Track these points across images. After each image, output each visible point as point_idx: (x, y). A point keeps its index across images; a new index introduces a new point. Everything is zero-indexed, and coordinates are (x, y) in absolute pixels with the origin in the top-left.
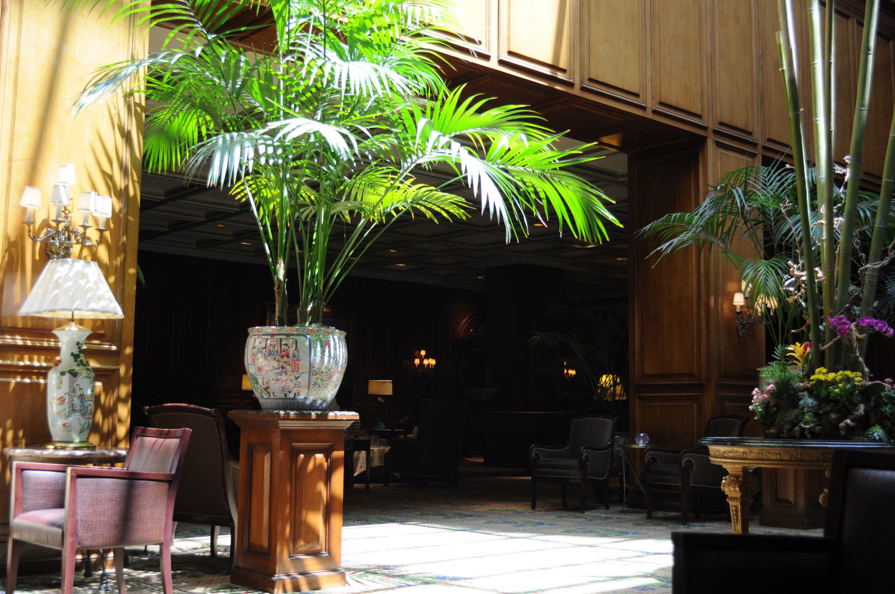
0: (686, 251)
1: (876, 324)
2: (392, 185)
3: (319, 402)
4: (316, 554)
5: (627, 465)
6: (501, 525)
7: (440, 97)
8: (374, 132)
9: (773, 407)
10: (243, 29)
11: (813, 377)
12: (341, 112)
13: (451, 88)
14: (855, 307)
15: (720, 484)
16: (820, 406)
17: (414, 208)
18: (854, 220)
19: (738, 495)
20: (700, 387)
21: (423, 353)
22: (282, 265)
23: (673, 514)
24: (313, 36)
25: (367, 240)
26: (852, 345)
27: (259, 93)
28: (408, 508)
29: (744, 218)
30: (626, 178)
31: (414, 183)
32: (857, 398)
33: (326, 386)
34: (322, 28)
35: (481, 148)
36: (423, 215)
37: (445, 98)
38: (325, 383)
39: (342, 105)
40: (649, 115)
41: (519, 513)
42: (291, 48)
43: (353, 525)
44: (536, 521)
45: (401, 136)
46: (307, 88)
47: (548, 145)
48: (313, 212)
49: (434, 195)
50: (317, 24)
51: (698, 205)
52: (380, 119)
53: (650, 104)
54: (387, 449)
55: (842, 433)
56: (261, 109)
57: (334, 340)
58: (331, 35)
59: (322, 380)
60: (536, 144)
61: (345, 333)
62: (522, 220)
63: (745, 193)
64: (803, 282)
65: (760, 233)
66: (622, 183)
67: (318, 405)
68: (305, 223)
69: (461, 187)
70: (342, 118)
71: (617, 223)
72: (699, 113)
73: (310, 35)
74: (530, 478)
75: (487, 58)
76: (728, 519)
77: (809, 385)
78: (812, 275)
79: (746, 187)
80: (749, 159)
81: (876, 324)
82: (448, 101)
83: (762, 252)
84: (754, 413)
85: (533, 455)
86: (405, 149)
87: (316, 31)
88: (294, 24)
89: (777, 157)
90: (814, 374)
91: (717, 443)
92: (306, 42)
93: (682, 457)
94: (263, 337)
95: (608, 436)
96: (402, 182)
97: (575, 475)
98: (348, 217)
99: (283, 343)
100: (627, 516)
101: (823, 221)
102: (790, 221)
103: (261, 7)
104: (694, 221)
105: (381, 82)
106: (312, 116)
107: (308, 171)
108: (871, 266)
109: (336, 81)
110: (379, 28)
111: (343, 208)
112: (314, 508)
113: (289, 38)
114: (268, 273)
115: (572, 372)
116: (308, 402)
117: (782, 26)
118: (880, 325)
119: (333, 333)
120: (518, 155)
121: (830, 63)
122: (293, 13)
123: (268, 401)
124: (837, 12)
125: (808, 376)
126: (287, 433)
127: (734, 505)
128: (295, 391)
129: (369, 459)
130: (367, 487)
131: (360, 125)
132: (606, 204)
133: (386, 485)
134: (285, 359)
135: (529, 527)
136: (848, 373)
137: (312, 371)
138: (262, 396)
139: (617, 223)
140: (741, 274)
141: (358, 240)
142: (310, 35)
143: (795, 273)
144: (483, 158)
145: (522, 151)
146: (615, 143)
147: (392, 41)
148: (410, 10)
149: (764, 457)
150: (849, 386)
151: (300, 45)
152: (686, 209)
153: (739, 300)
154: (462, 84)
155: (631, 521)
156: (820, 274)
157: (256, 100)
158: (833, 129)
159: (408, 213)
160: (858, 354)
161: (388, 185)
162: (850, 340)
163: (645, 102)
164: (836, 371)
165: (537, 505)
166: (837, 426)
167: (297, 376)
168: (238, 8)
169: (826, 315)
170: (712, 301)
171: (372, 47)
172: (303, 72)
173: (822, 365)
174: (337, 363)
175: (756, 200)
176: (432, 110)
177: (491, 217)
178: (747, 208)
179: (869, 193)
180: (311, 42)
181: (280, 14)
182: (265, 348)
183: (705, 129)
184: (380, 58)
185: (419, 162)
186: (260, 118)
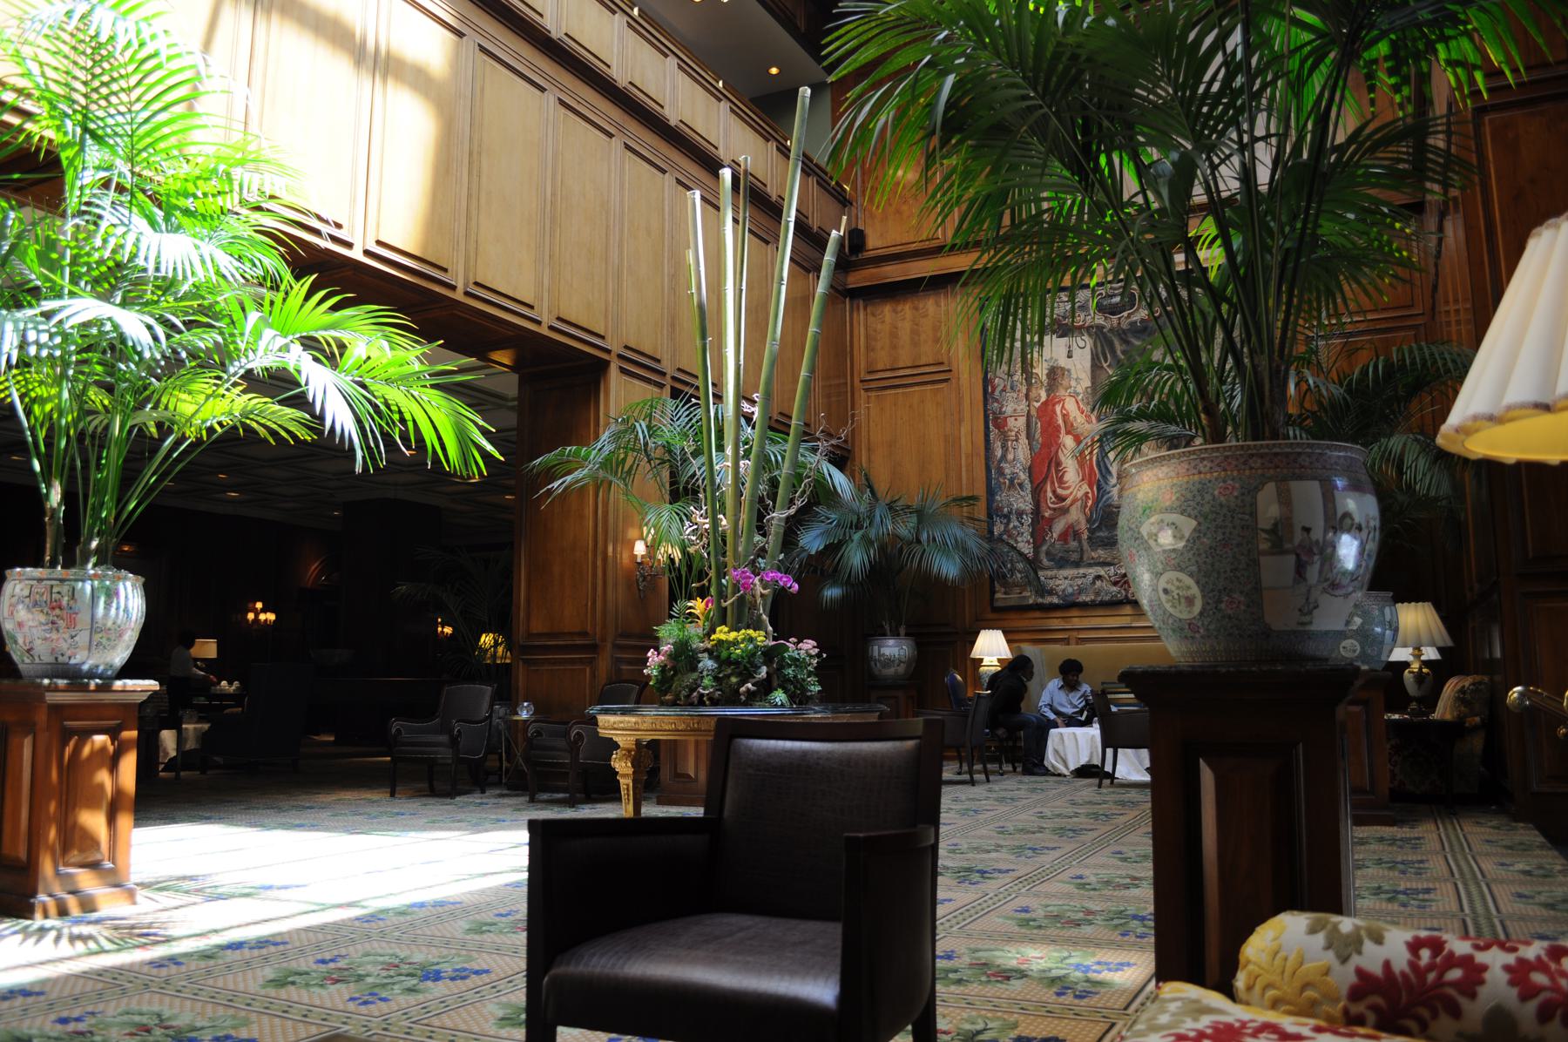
0: (582, 491)
1: (781, 578)
2: (214, 391)
3: (101, 668)
4: (94, 866)
5: (507, 740)
6: (350, 818)
7: (282, 288)
8: (189, 325)
9: (670, 670)
10: (16, 176)
11: (713, 637)
12: (149, 296)
13: (298, 278)
14: (760, 560)
15: (610, 760)
16: (720, 669)
17: (243, 424)
18: (764, 463)
19: (630, 771)
20: (594, 648)
21: (259, 605)
22: (59, 489)
23: (561, 796)
24: (116, 195)
25: (178, 460)
26: (756, 601)
27: (36, 260)
28: (231, 801)
29: (648, 456)
30: (516, 403)
31: (244, 392)
32: (759, 659)
33: (114, 647)
34: (129, 186)
35: (333, 354)
36: (255, 432)
37: (947, 248)
38: (112, 643)
39: (150, 287)
40: (544, 331)
41: (373, 802)
42: (84, 208)
43: (155, 825)
44: (492, 817)
45: (227, 331)
46: (101, 262)
47: (417, 357)
48: (106, 421)
49: (269, 408)
50: (121, 180)
51: (597, 437)
52: (202, 310)
53: (547, 319)
54: (206, 726)
55: (743, 698)
56: (39, 283)
57: (126, 589)
58: (140, 196)
59: (108, 639)
60: (400, 353)
61: (143, 579)
62: (378, 446)
63: (649, 428)
64: (706, 530)
65: (666, 474)
66: (512, 408)
67: (100, 671)
68: (93, 436)
69: (300, 401)
70: (147, 304)
71: (497, 455)
72: (602, 334)
73: (112, 194)
74: (389, 759)
75: (349, 245)
76: (619, 799)
77: (709, 646)
78: (715, 523)
79: (650, 421)
80: (656, 390)
81: (781, 578)
82: (292, 294)
83: (667, 497)
84: (649, 677)
85: (394, 731)
86: (232, 347)
87: (121, 189)
88: (89, 177)
89: (686, 389)
90: (715, 633)
91: (606, 712)
92: (106, 202)
93: (571, 728)
94: (27, 582)
95: (485, 705)
96: (228, 390)
97: (444, 754)
98: (153, 430)
99: (55, 590)
100: (506, 801)
101: (729, 464)
102: (696, 463)
103: (47, 151)
104: (592, 457)
105: (203, 262)
106: (106, 297)
107: (99, 368)
108: (778, 516)
109: (142, 255)
110: (205, 195)
111: (149, 419)
112: (93, 804)
113: (80, 196)
114: (40, 500)
115: (448, 630)
116: (85, 667)
117: (692, 245)
118: (785, 579)
119: (126, 578)
120: (380, 366)
121: (741, 290)
122: (89, 164)
123: (31, 667)
124: (750, 231)
125: (708, 635)
126: (57, 709)
127: (625, 783)
128: (69, 653)
129: (180, 741)
130: (178, 775)
131: (174, 315)
132: (485, 432)
133: (203, 772)
134: (57, 611)
135: (385, 818)
136: (751, 632)
137: (94, 628)
138: (23, 661)
139: (497, 455)
140: (643, 519)
141: (162, 463)
142: (112, 194)
143: (698, 519)
144: (335, 366)
145: (385, 361)
146: (506, 361)
147: (222, 213)
148: (247, 177)
149: (658, 727)
150: (751, 647)
151: (98, 206)
152: (583, 441)
153: (640, 549)
154: (312, 274)
155: (510, 806)
156: (724, 522)
157: (34, 273)
158: (742, 362)
159: (235, 428)
160: (761, 611)
161: (209, 392)
162: (754, 596)
163: (541, 316)
164: (738, 630)
165: (397, 792)
166: (737, 691)
167: (74, 634)
168: (10, 148)
169: (730, 568)
170: (610, 549)
171: (195, 217)
172: (98, 242)
173: (724, 623)
174: (128, 617)
175: (662, 436)
176: (272, 303)
177: (337, 440)
178: (651, 445)
179: (782, 435)
180: (113, 203)
181: (71, 162)
182: (29, 596)
183: (608, 351)
184: (205, 232)
185: (249, 366)
186: (35, 292)
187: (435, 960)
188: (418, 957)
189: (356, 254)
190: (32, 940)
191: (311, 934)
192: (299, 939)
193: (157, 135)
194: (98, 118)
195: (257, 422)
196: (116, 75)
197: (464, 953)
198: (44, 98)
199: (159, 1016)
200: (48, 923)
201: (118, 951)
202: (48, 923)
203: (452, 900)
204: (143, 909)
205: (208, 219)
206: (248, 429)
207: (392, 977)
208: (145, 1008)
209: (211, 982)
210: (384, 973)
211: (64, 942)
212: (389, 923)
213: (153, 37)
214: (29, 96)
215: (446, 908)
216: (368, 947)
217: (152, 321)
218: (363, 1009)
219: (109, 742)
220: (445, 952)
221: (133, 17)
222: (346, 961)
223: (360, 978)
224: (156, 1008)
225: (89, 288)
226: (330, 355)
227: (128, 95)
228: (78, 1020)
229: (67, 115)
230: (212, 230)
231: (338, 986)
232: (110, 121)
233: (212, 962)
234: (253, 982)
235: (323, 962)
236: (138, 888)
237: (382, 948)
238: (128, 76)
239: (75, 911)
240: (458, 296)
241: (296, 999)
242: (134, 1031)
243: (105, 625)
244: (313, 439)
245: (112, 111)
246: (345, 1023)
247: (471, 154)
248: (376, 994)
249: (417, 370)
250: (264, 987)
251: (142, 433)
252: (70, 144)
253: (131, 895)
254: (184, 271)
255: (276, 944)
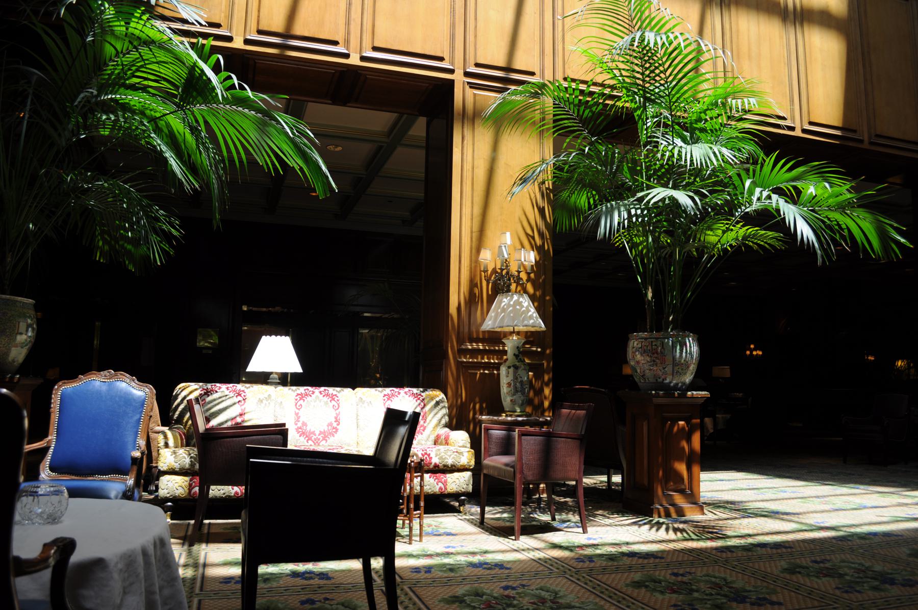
4: (682, 492)
13: (767, 155)
21: (752, 346)
31: (743, 226)
33: (685, 374)
38: (684, 371)
39: (687, 175)
47: (847, 190)
54: (728, 416)
59: (682, 369)
60: (837, 189)
71: (908, 244)
87: (666, 126)
92: (659, 134)
106: (665, 186)
112: (680, 459)
119: (688, 337)
120: (823, 199)
129: (715, 424)
138: (640, 381)
139: (908, 244)
145: (826, 195)
146: (898, 181)
159: (739, 247)
174: (692, 358)
180: (662, 133)
181: (640, 117)
187: (890, 571)
188: (878, 568)
189: (798, 133)
190: (654, 529)
191: (806, 544)
192: (800, 547)
193: (682, 91)
194: (651, 90)
195: (752, 242)
196: (657, 65)
197: (909, 569)
198: (623, 87)
199: (725, 580)
200: (661, 520)
201: (698, 540)
202: (661, 520)
203: (895, 534)
204: (708, 516)
205: (714, 131)
206: (746, 246)
207: (861, 578)
208: (717, 574)
209: (751, 565)
210: (856, 575)
211: (671, 532)
212: (855, 543)
213: (676, 38)
214: (615, 88)
215: (893, 538)
216: (843, 556)
217: (691, 194)
218: (845, 595)
219: (686, 425)
220: (895, 567)
221: (663, 31)
222: (831, 564)
223: (841, 576)
224: (723, 575)
225: (655, 181)
226: (794, 197)
227: (665, 74)
228: (682, 575)
229: (635, 93)
230: (717, 137)
231: (827, 579)
232: (657, 90)
233: (750, 553)
234: (776, 567)
235: (816, 562)
236: (704, 506)
237: (853, 559)
238: (664, 64)
239: (674, 515)
240: (866, 146)
241: (802, 582)
242: (712, 586)
243: (680, 361)
244: (785, 248)
245: (657, 85)
246: (835, 602)
247: (863, 54)
248: (853, 588)
249: (849, 197)
250: (782, 572)
251: (689, 254)
252: (638, 108)
253: (702, 509)
254: (706, 163)
255: (786, 547)
